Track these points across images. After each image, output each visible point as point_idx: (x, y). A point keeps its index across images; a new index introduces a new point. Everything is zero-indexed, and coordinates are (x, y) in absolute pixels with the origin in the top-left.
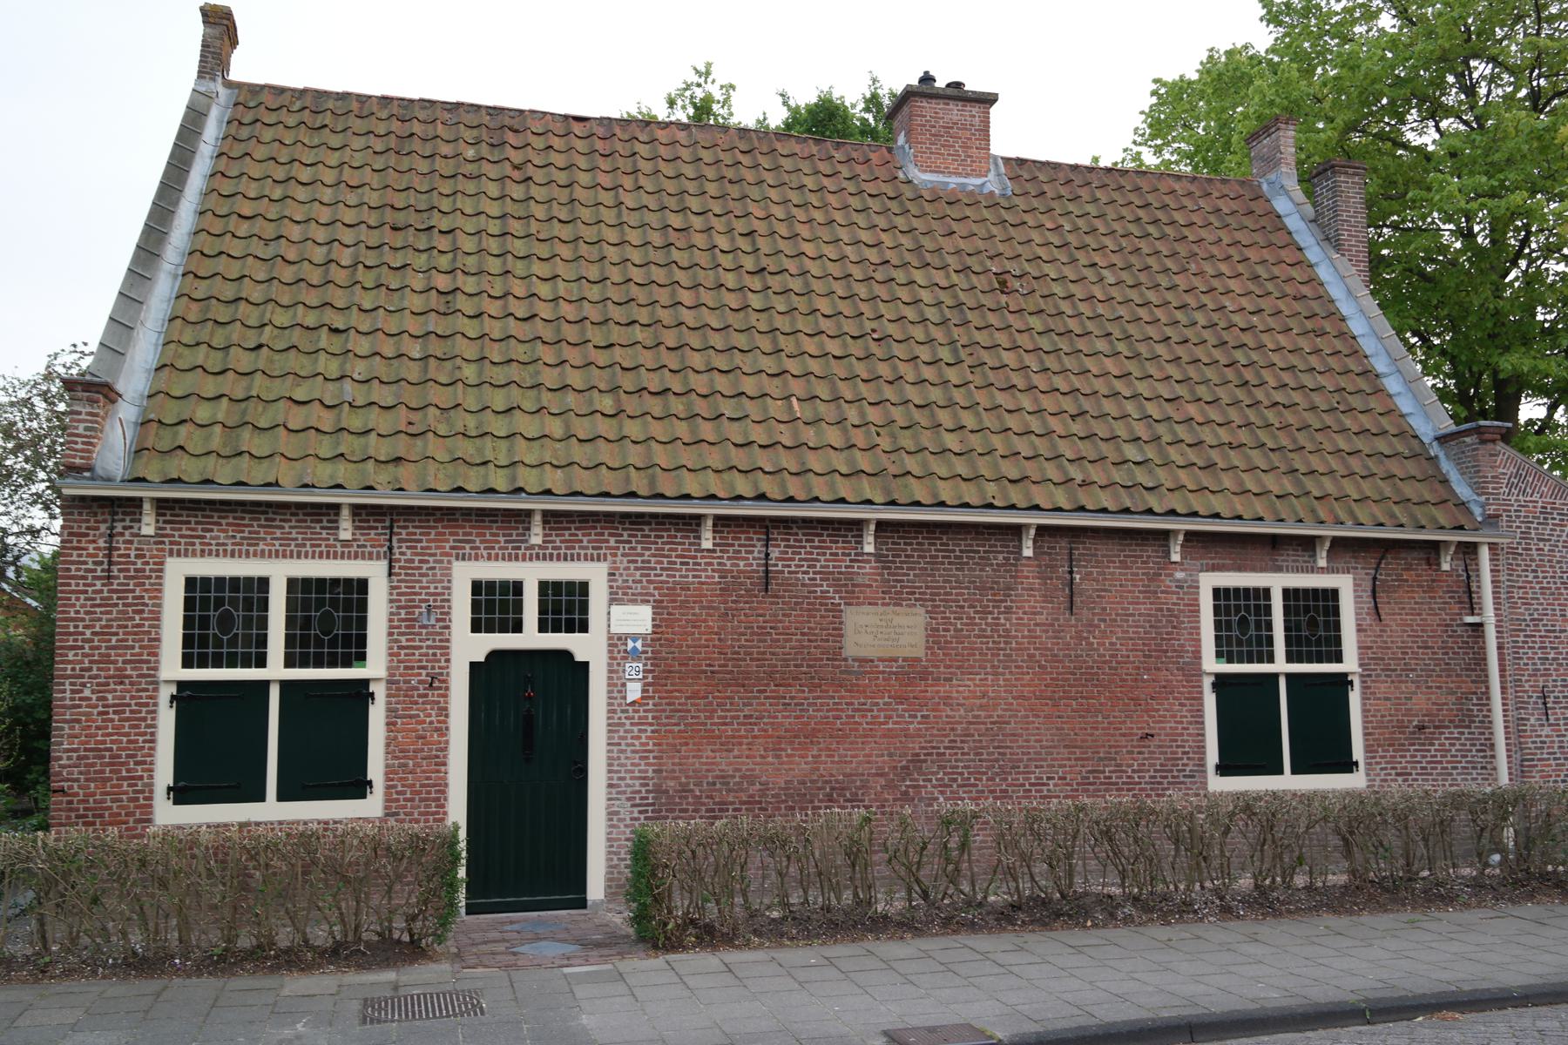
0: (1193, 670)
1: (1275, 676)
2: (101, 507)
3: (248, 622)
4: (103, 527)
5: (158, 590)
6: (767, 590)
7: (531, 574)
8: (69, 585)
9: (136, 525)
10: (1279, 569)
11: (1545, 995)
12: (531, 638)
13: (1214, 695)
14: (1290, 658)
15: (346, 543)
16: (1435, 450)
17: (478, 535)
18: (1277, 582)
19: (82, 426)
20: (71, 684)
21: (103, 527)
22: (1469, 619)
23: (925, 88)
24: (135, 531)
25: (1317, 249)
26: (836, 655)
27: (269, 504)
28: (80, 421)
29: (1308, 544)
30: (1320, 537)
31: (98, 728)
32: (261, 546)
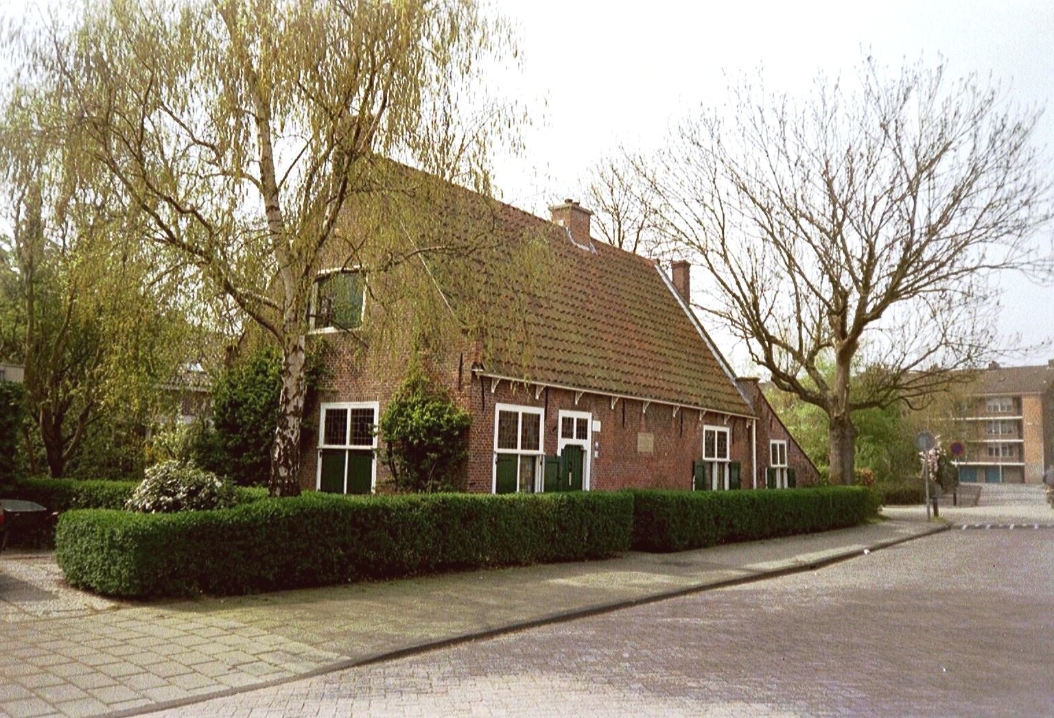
0: (492, 451)
7: (576, 415)
10: (716, 425)
12: (574, 441)
14: (353, 442)
18: (521, 410)
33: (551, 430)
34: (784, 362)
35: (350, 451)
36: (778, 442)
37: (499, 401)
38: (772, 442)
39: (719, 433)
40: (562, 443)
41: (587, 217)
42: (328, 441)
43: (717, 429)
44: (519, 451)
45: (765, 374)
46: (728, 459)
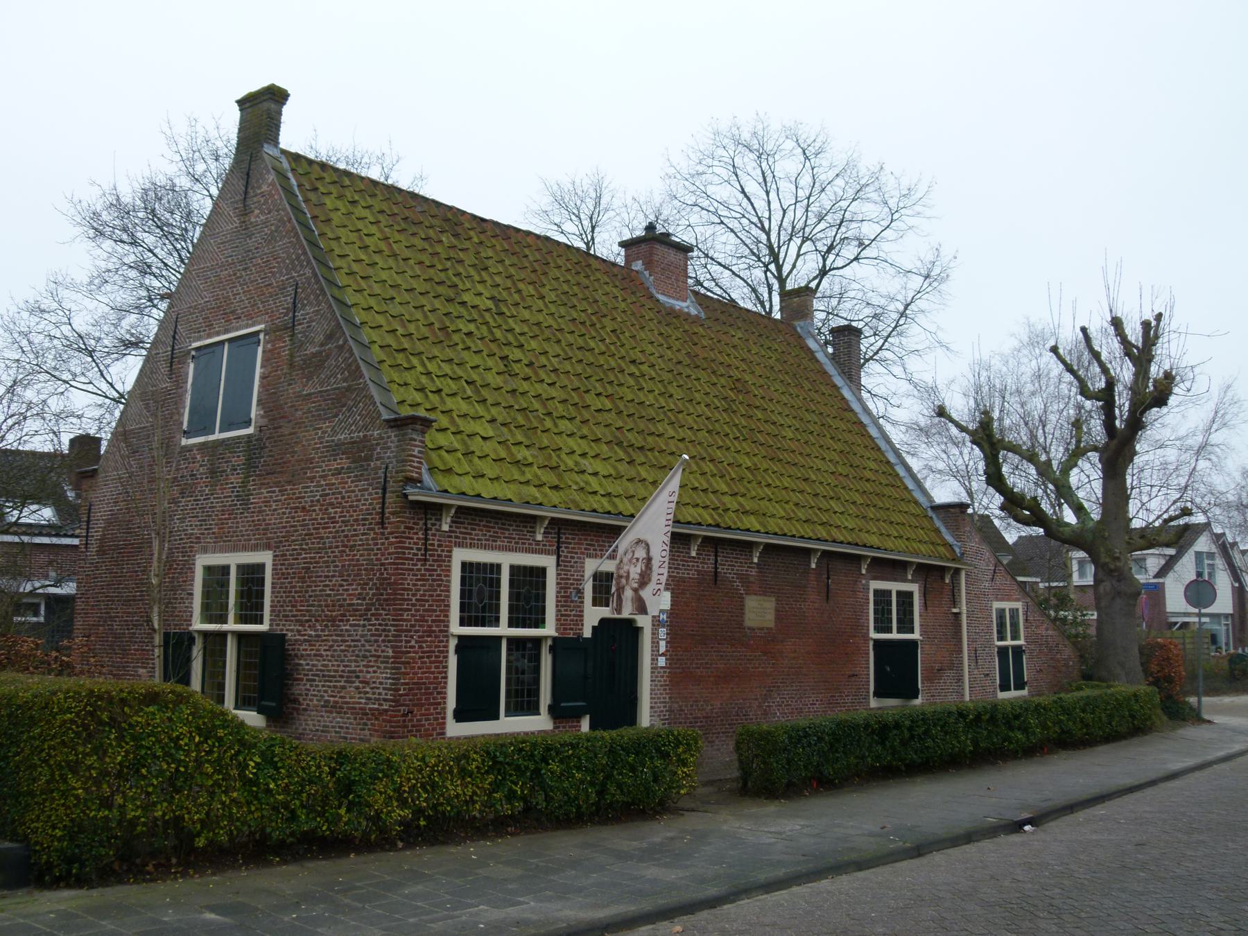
0: (866, 637)
1: (499, 638)
2: (419, 508)
3: (491, 598)
4: (421, 523)
5: (448, 570)
6: (716, 584)
8: (404, 564)
9: (438, 523)
10: (895, 580)
11: (944, 840)
13: (456, 657)
14: (512, 623)
15: (538, 543)
16: (930, 513)
17: (597, 541)
18: (506, 560)
19: (417, 449)
20: (406, 636)
21: (421, 523)
22: (955, 610)
23: (651, 235)
24: (437, 527)
25: (839, 378)
26: (740, 625)
27: (503, 513)
28: (416, 446)
29: (904, 565)
30: (813, 549)
31: (419, 668)
32: (498, 543)
33: (570, 598)
34: (1021, 478)
35: (512, 641)
36: (1007, 605)
37: (460, 545)
38: (997, 605)
39: (899, 593)
40: (593, 616)
41: (681, 256)
42: (878, 630)
43: (894, 587)
44: (503, 629)
45: (990, 503)
46: (549, 630)
